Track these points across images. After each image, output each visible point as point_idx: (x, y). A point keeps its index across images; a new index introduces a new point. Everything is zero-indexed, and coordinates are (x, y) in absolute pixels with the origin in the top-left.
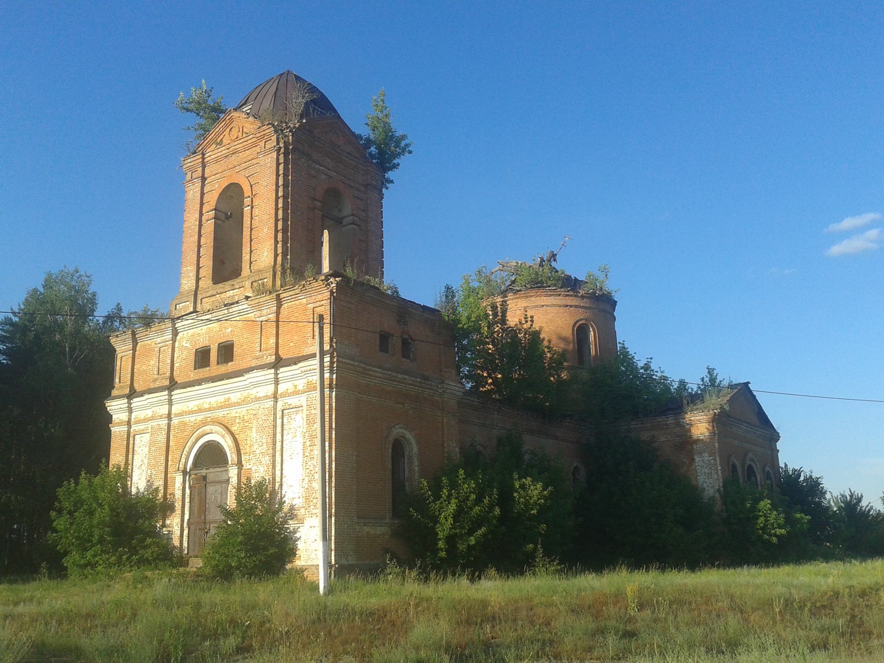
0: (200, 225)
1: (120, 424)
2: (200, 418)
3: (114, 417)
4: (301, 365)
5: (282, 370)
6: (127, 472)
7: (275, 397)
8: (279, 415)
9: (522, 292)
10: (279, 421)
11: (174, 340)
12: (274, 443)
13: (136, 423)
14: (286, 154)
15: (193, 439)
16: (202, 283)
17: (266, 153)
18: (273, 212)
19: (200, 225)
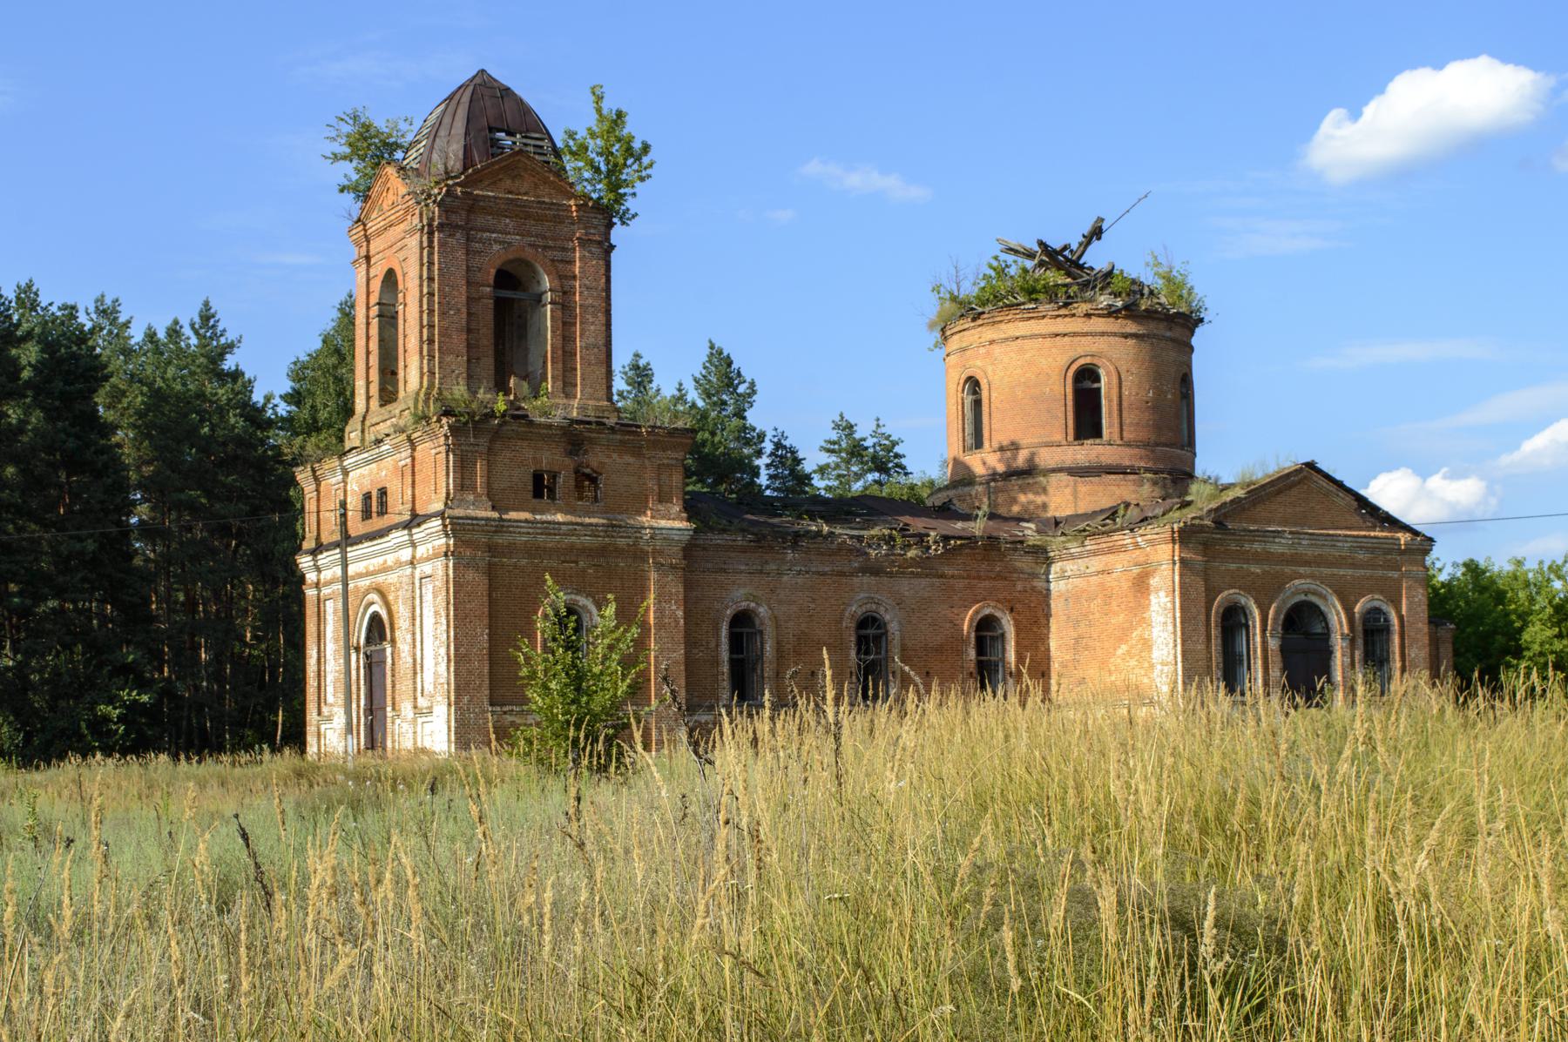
2: (368, 583)
3: (308, 576)
5: (414, 531)
8: (417, 585)
9: (985, 316)
10: (418, 591)
11: (345, 482)
12: (414, 619)
14: (431, 234)
15: (361, 610)
17: (411, 232)
18: (418, 315)
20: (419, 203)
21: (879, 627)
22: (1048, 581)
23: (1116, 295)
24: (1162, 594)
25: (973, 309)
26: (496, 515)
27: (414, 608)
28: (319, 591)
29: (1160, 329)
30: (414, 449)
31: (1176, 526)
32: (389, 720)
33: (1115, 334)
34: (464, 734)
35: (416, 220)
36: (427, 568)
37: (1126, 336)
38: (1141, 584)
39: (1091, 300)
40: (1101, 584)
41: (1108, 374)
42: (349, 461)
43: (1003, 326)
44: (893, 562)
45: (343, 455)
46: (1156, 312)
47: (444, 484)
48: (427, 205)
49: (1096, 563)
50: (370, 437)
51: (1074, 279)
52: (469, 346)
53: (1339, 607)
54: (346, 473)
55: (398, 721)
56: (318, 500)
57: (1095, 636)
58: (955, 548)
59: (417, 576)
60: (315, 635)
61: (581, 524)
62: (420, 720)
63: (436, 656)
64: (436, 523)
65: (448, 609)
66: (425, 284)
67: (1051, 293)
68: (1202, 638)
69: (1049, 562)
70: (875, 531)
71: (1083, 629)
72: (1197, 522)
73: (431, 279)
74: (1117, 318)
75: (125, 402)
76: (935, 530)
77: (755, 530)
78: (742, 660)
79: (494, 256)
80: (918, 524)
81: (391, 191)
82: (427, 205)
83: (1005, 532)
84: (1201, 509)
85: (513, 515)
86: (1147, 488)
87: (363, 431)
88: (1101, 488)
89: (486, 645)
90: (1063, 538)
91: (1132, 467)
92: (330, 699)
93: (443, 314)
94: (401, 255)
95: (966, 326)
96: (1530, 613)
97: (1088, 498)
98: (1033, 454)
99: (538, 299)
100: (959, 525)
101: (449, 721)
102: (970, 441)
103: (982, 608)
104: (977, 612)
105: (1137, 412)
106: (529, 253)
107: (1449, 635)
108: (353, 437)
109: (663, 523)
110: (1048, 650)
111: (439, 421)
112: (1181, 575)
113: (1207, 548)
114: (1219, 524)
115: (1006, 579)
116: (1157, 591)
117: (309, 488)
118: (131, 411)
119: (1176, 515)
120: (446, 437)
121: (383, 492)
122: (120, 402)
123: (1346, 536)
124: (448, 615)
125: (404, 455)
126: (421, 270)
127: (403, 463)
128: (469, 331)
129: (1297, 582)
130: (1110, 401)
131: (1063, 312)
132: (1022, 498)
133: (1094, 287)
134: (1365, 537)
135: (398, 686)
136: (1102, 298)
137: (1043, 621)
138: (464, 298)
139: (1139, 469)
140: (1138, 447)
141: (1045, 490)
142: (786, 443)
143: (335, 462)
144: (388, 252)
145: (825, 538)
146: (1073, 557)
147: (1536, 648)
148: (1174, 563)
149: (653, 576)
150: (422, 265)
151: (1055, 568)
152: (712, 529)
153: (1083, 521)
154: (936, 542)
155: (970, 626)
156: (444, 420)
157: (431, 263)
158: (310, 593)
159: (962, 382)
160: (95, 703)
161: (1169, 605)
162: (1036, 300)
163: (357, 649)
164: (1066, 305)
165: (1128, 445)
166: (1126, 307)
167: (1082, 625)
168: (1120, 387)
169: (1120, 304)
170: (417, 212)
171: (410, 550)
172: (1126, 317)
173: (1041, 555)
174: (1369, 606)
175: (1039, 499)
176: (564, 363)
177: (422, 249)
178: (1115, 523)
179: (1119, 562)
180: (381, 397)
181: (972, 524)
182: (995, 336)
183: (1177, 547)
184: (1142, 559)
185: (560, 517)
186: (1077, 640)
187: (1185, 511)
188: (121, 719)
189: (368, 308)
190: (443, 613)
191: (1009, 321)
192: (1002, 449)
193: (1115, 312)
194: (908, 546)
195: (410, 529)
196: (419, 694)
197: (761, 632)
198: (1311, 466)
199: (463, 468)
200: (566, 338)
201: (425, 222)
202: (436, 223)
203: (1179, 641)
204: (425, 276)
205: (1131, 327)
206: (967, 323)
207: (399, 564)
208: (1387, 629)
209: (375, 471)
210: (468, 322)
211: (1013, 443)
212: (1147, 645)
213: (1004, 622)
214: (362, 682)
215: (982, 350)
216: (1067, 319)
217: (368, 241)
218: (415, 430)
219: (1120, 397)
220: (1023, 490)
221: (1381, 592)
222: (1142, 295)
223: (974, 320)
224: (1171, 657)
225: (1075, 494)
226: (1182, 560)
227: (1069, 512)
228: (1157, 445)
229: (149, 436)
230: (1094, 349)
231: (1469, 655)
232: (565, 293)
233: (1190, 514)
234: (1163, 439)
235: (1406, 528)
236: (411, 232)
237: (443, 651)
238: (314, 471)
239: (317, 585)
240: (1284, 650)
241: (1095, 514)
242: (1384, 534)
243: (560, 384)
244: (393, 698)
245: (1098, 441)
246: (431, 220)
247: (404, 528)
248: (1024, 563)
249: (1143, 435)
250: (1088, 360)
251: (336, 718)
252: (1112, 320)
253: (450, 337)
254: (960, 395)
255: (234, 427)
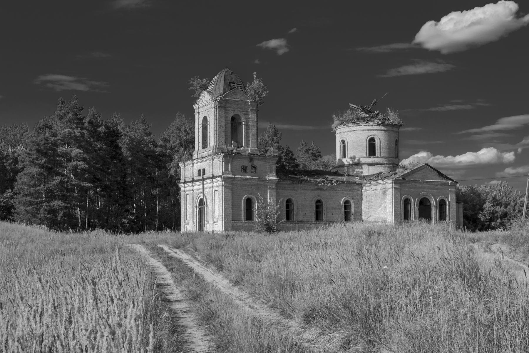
0: (199, 129)
1: (183, 191)
2: (199, 191)
3: (182, 189)
4: (216, 179)
5: (213, 180)
6: (144, 324)
7: (213, 187)
10: (214, 194)
13: (187, 191)
14: (216, 109)
15: (198, 197)
16: (200, 148)
17: (211, 108)
18: (213, 128)
19: (199, 129)
20: (213, 101)
21: (321, 203)
22: (362, 192)
23: (379, 120)
24: (390, 196)
25: (343, 123)
26: (234, 176)
27: (213, 197)
28: (185, 192)
29: (390, 128)
30: (213, 160)
31: (393, 180)
32: (206, 224)
33: (379, 130)
34: (226, 228)
35: (213, 105)
36: (217, 189)
37: (382, 130)
38: (384, 193)
39: (373, 121)
40: (375, 193)
41: (377, 140)
42: (194, 162)
43: (351, 127)
44: (324, 187)
45: (192, 160)
46: (389, 124)
47: (222, 169)
48: (216, 102)
49: (374, 188)
50: (200, 156)
51: (369, 115)
52: (225, 135)
53: (433, 199)
54: (193, 164)
55: (208, 224)
56: (185, 170)
57: (373, 205)
58: (339, 184)
59: (214, 190)
60: (184, 203)
61: (253, 178)
62: (214, 224)
63: (219, 209)
64: (220, 178)
65: (222, 198)
66: (215, 120)
67: (363, 119)
68: (399, 206)
69: (362, 187)
70: (320, 180)
71: (370, 204)
72: (398, 178)
73: (216, 119)
74: (380, 126)
75: (124, 141)
76: (334, 179)
77: (292, 179)
78: (288, 211)
79: (231, 114)
80: (330, 177)
81: (205, 98)
82: (216, 102)
83: (351, 180)
84: (399, 175)
85: (237, 176)
86: (387, 168)
87: (198, 155)
88: (375, 169)
89: (231, 207)
90: (366, 181)
91: (383, 163)
92: (188, 218)
93: (219, 128)
94: (208, 113)
95: (342, 127)
96: (486, 199)
97: (372, 171)
98: (359, 159)
99: (241, 123)
100: (340, 177)
101: (223, 224)
102: (342, 156)
103: (346, 198)
104: (344, 199)
105: (384, 149)
106: (239, 113)
107: (462, 206)
108: (195, 156)
109: (271, 178)
110: (362, 208)
111: (221, 154)
112: (394, 191)
113: (400, 184)
114: (404, 179)
115: (351, 191)
116: (388, 195)
117: (182, 168)
118: (125, 144)
119: (393, 176)
120: (222, 158)
121: (204, 170)
122: (122, 141)
123: (435, 182)
124: (222, 200)
125: (210, 161)
126: (214, 117)
127: (210, 163)
128: (225, 132)
129: (422, 193)
130: (378, 147)
131: (366, 124)
132: (356, 170)
133: (374, 118)
134: (440, 182)
135: (208, 216)
136: (376, 121)
137: (360, 202)
138: (224, 124)
139: (385, 163)
140: (384, 158)
141: (362, 168)
142: (290, 150)
143: (191, 162)
144: (205, 112)
145: (309, 181)
146: (368, 186)
147: (487, 209)
148: (393, 188)
149: (269, 191)
150: (214, 116)
151: (364, 188)
152: (282, 179)
153: (370, 177)
154: (335, 182)
155: (343, 202)
156: (222, 154)
157: (216, 116)
158: (182, 193)
159: (340, 141)
160: (121, 219)
161: (391, 198)
162: (359, 121)
163: (196, 207)
164: (367, 123)
165: (382, 158)
166: (382, 123)
167: (370, 202)
168: (380, 143)
169: (380, 122)
170: (213, 103)
171: (212, 184)
172: (382, 126)
173: (360, 185)
174: (441, 199)
175: (361, 170)
176: (247, 139)
177: (214, 112)
178: (378, 178)
179: (379, 187)
180: (202, 147)
181: (343, 177)
182: (349, 130)
183: (393, 184)
184: (385, 187)
185: (248, 177)
186: (369, 206)
187: (395, 175)
188: (128, 223)
189: (199, 125)
190: (221, 199)
191: (353, 126)
192: (351, 158)
193: (379, 124)
194: (327, 183)
195: (212, 179)
196: (214, 218)
197: (293, 204)
198: (427, 164)
199: (226, 165)
200: (248, 133)
201: (215, 106)
202: (218, 106)
203: (393, 207)
204: (215, 119)
205: (383, 128)
206: (342, 126)
207: (209, 188)
208: (445, 204)
209: (202, 164)
210: (225, 129)
211: (354, 156)
212: (386, 208)
213: (351, 201)
214: (198, 215)
215: (346, 133)
216: (367, 126)
217: (199, 108)
218: (214, 156)
219: (380, 146)
220: (357, 168)
221: (444, 195)
222: (386, 120)
223: (344, 126)
224: (392, 211)
225: (369, 170)
226: (395, 188)
227: (367, 174)
228: (389, 157)
229: (130, 150)
230: (374, 133)
231: (470, 210)
232: (247, 122)
233: (396, 176)
234: (391, 156)
235: (450, 179)
236: (211, 108)
237: (221, 208)
238: (184, 163)
239: (185, 191)
240: (419, 209)
241: (374, 175)
242: (445, 181)
243: (246, 144)
244: (207, 219)
245: (374, 157)
246: (217, 105)
247: (211, 179)
248: (356, 187)
249: (386, 155)
250: (372, 136)
251: (190, 223)
252: (378, 126)
253: (221, 133)
254: (340, 144)
255: (150, 148)
